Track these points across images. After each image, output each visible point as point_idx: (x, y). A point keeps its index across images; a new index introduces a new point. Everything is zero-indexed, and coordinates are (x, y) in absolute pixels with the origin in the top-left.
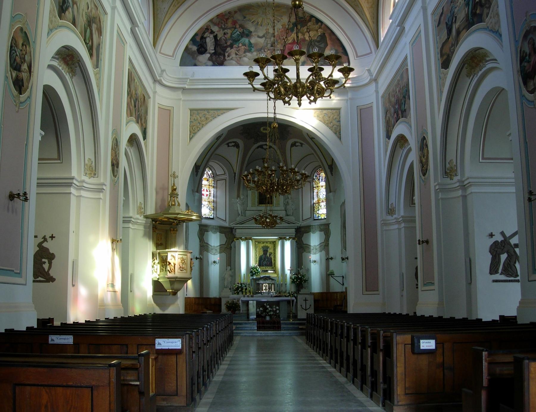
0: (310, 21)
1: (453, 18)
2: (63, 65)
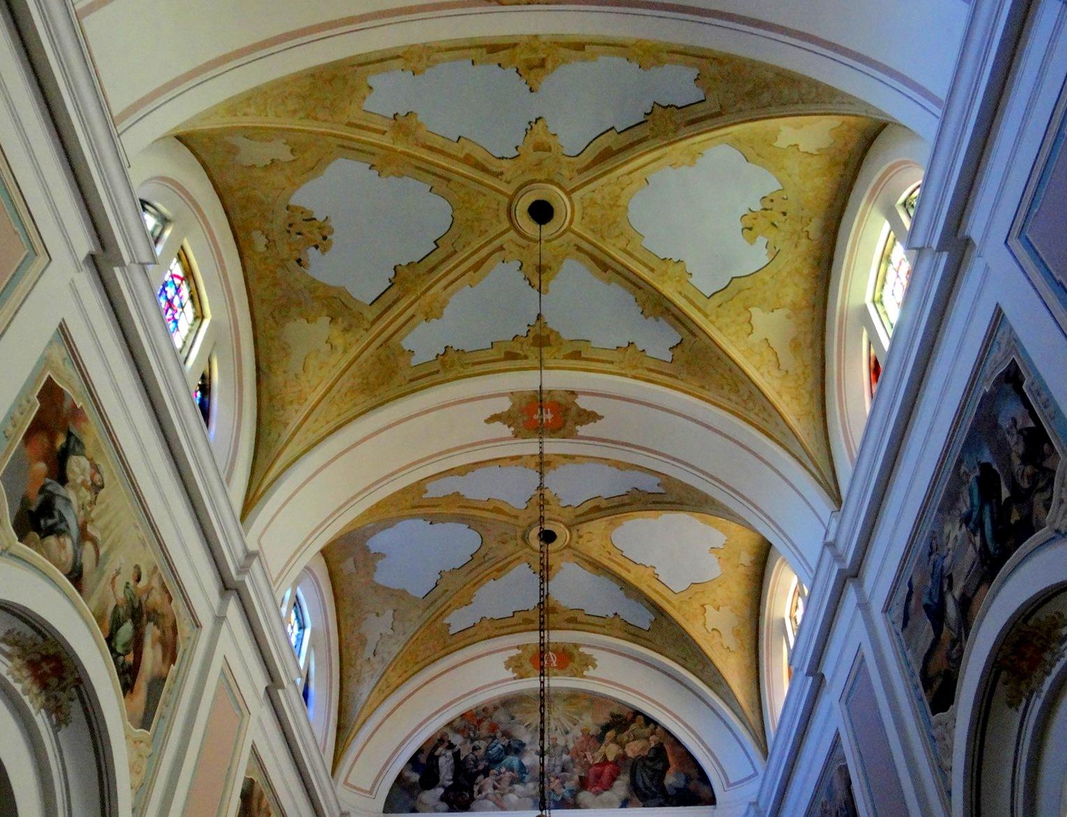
0: (633, 721)
1: (943, 579)
2: (28, 682)
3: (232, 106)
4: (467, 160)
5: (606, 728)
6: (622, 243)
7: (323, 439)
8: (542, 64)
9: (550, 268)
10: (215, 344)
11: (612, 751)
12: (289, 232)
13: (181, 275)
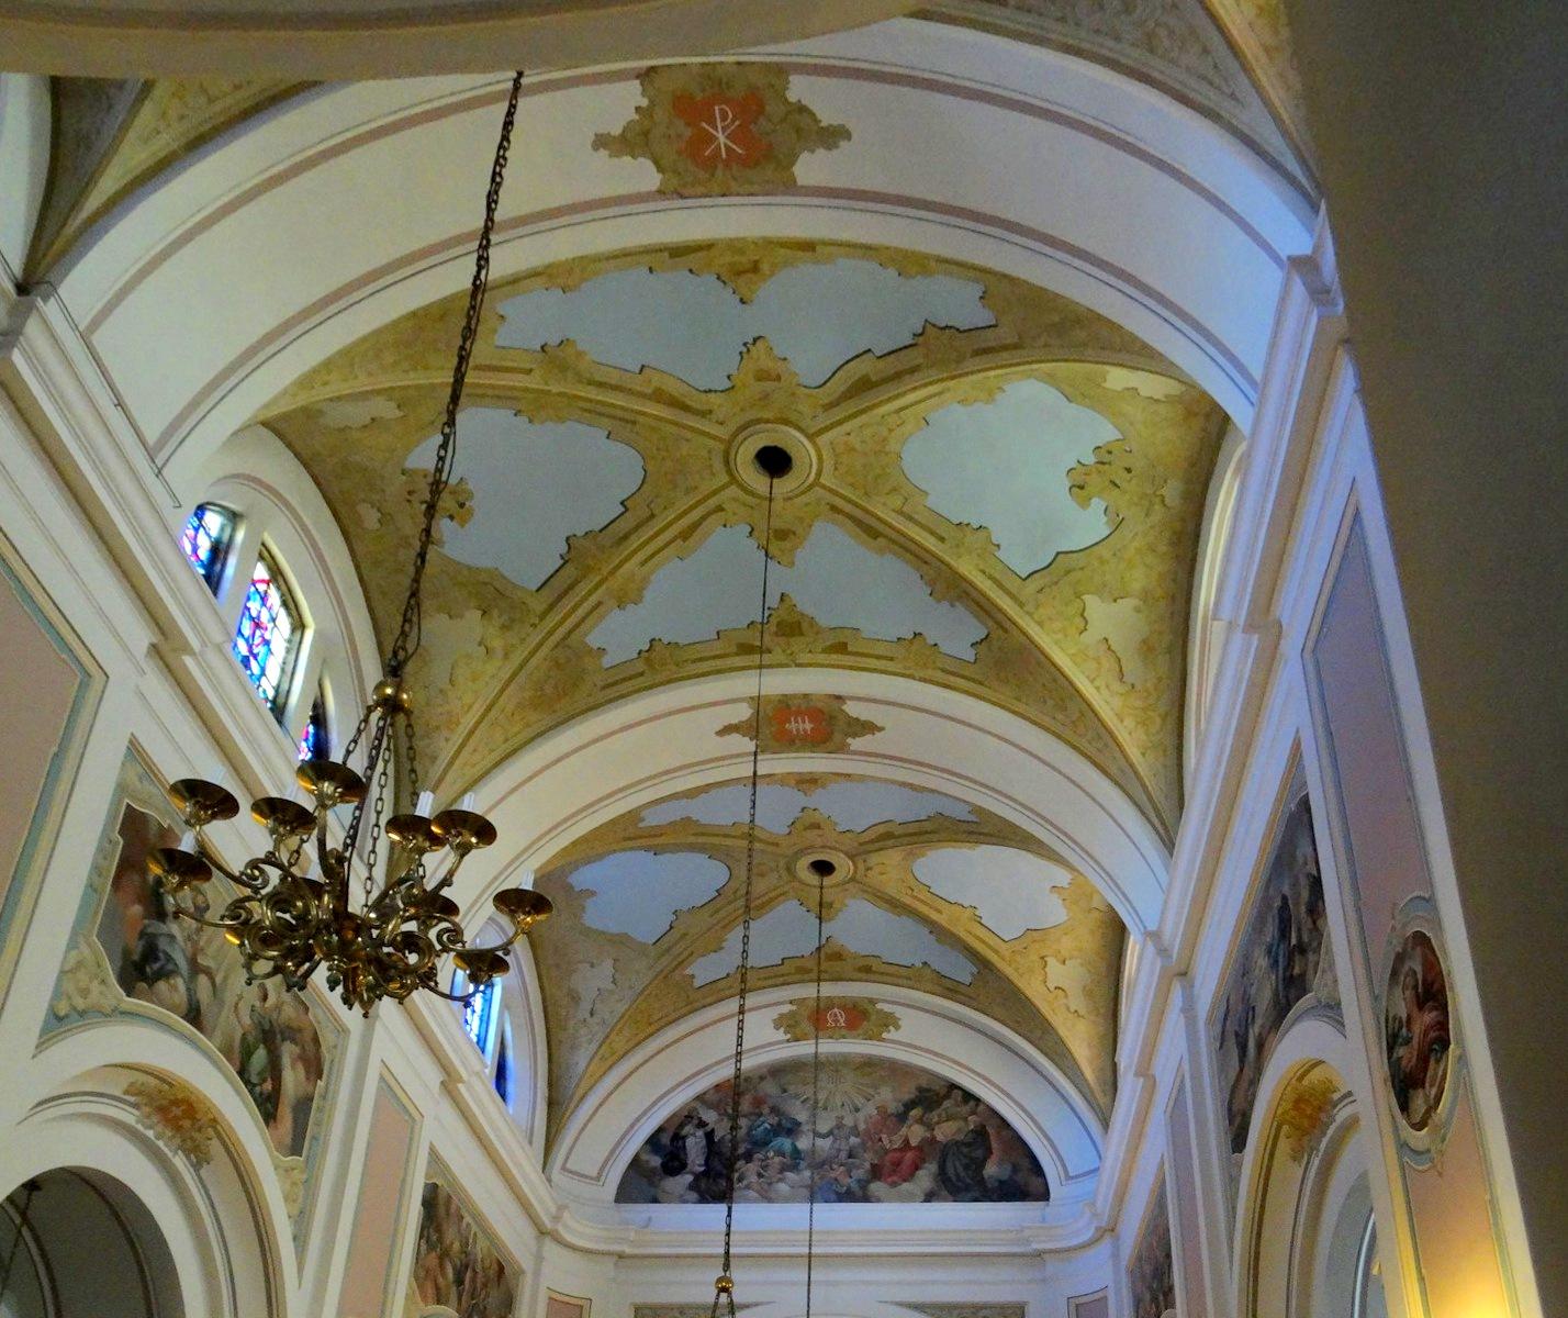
0: (947, 1096)
2: (160, 1128)
3: (306, 381)
4: (659, 396)
5: (910, 1105)
6: (897, 502)
7: (487, 772)
8: (755, 268)
9: (794, 533)
10: (324, 661)
11: (916, 1133)
12: (409, 501)
13: (267, 577)
